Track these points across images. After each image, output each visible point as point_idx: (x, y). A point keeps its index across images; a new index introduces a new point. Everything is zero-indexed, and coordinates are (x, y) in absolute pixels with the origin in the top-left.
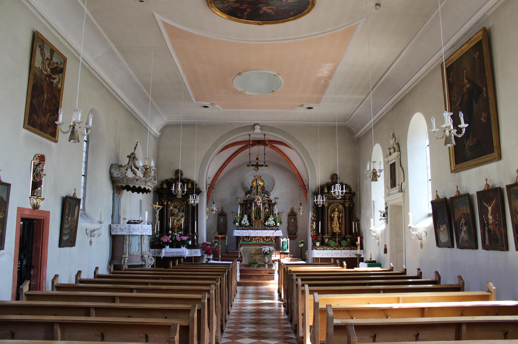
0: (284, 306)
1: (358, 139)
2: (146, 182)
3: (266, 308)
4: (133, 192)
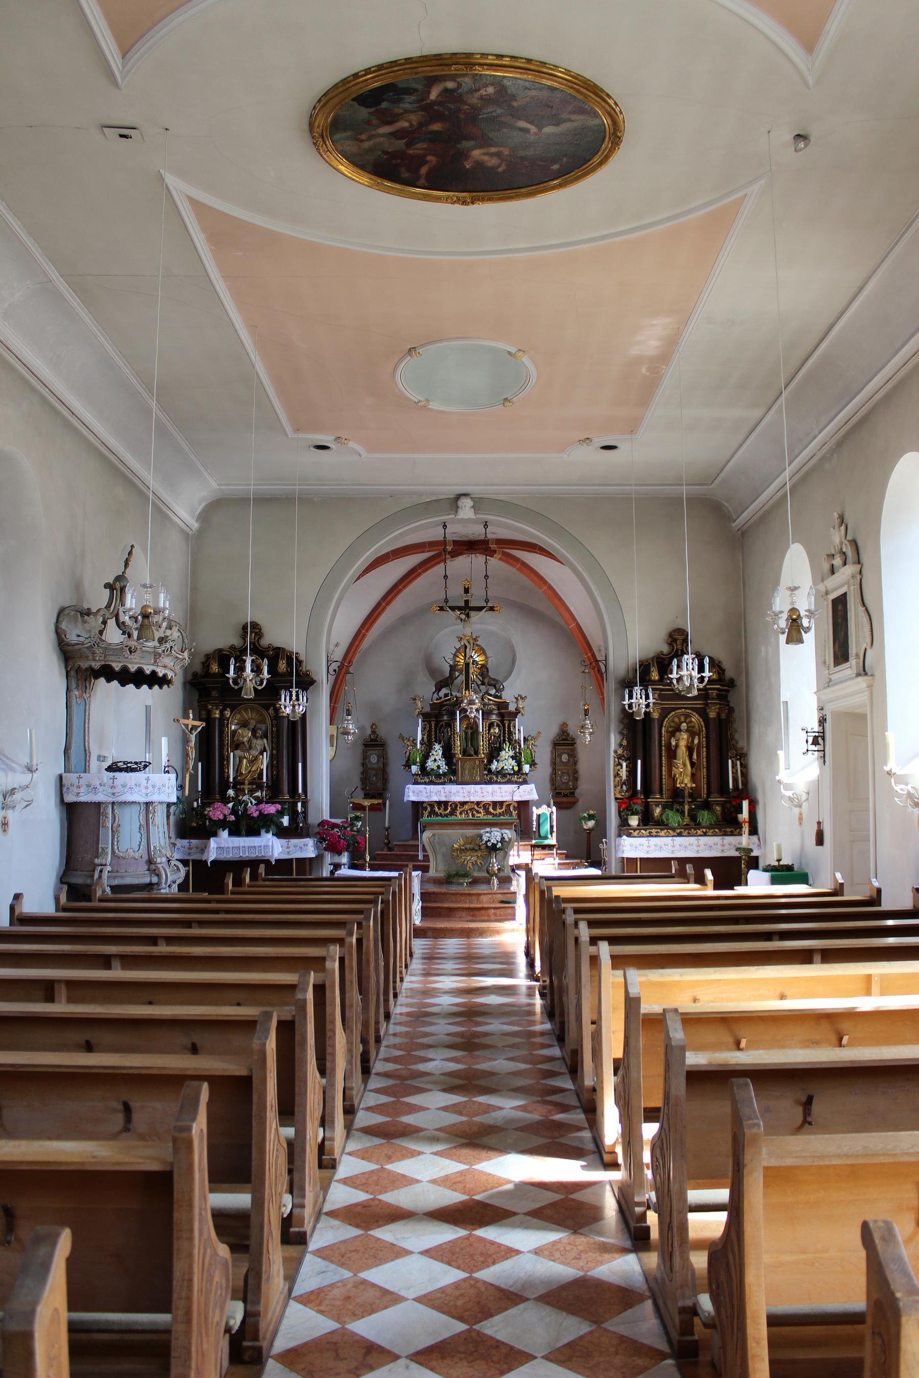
0: (542, 995)
1: (743, 534)
2: (157, 656)
3: (494, 1000)
4: (123, 684)
